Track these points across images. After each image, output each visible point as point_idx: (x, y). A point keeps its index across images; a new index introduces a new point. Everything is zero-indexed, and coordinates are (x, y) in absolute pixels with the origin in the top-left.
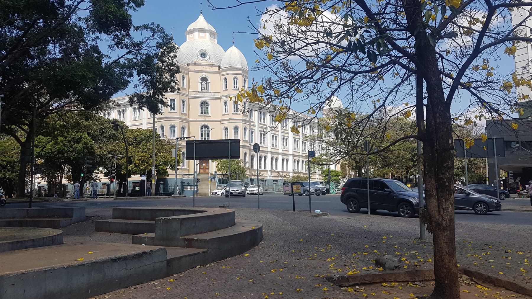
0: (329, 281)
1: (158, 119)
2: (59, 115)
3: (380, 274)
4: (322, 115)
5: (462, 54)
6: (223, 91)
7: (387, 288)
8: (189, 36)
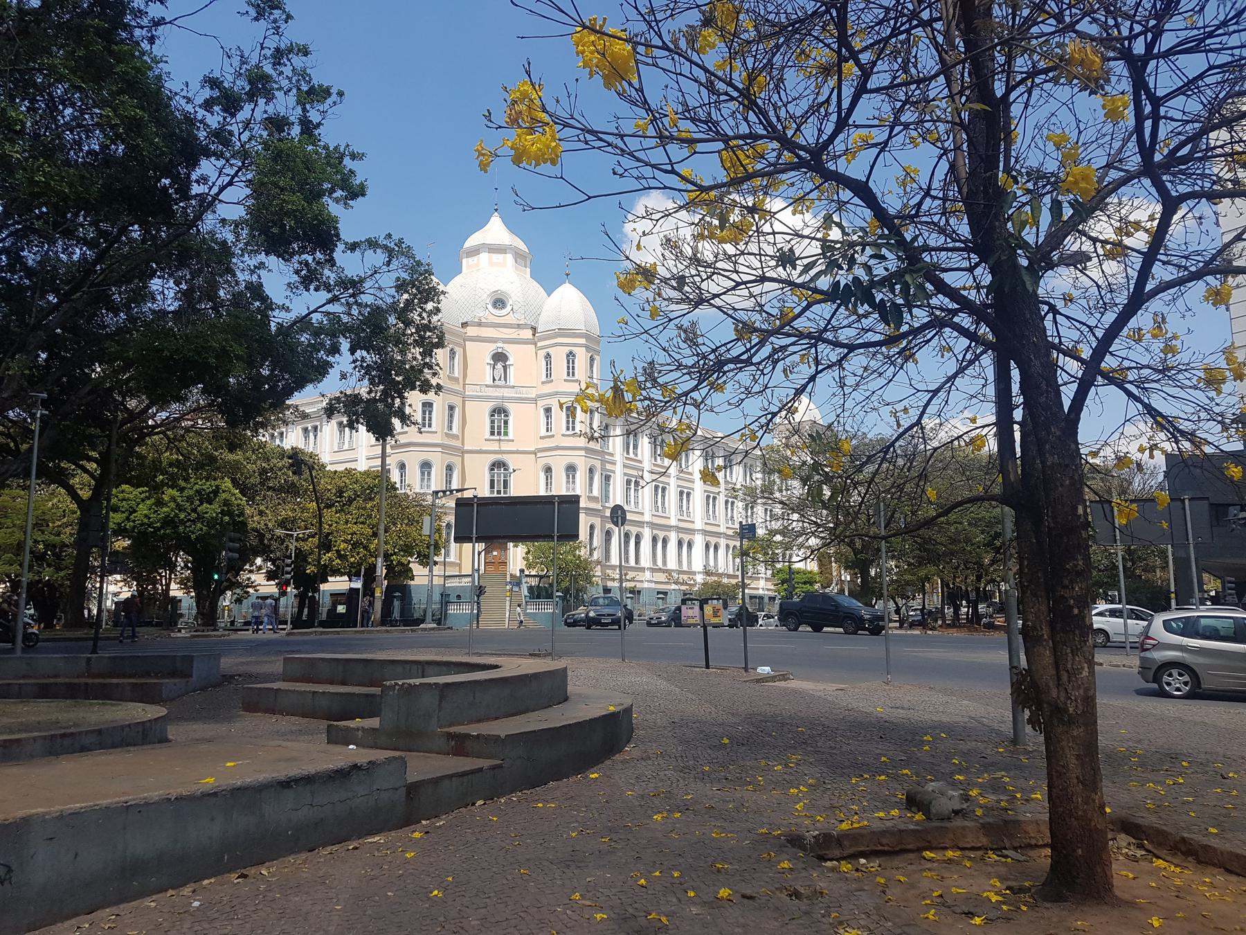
0: (794, 846)
1: (392, 447)
2: (168, 438)
3: (917, 830)
4: (772, 440)
5: (1101, 302)
6: (543, 383)
7: (935, 864)
8: (468, 262)
